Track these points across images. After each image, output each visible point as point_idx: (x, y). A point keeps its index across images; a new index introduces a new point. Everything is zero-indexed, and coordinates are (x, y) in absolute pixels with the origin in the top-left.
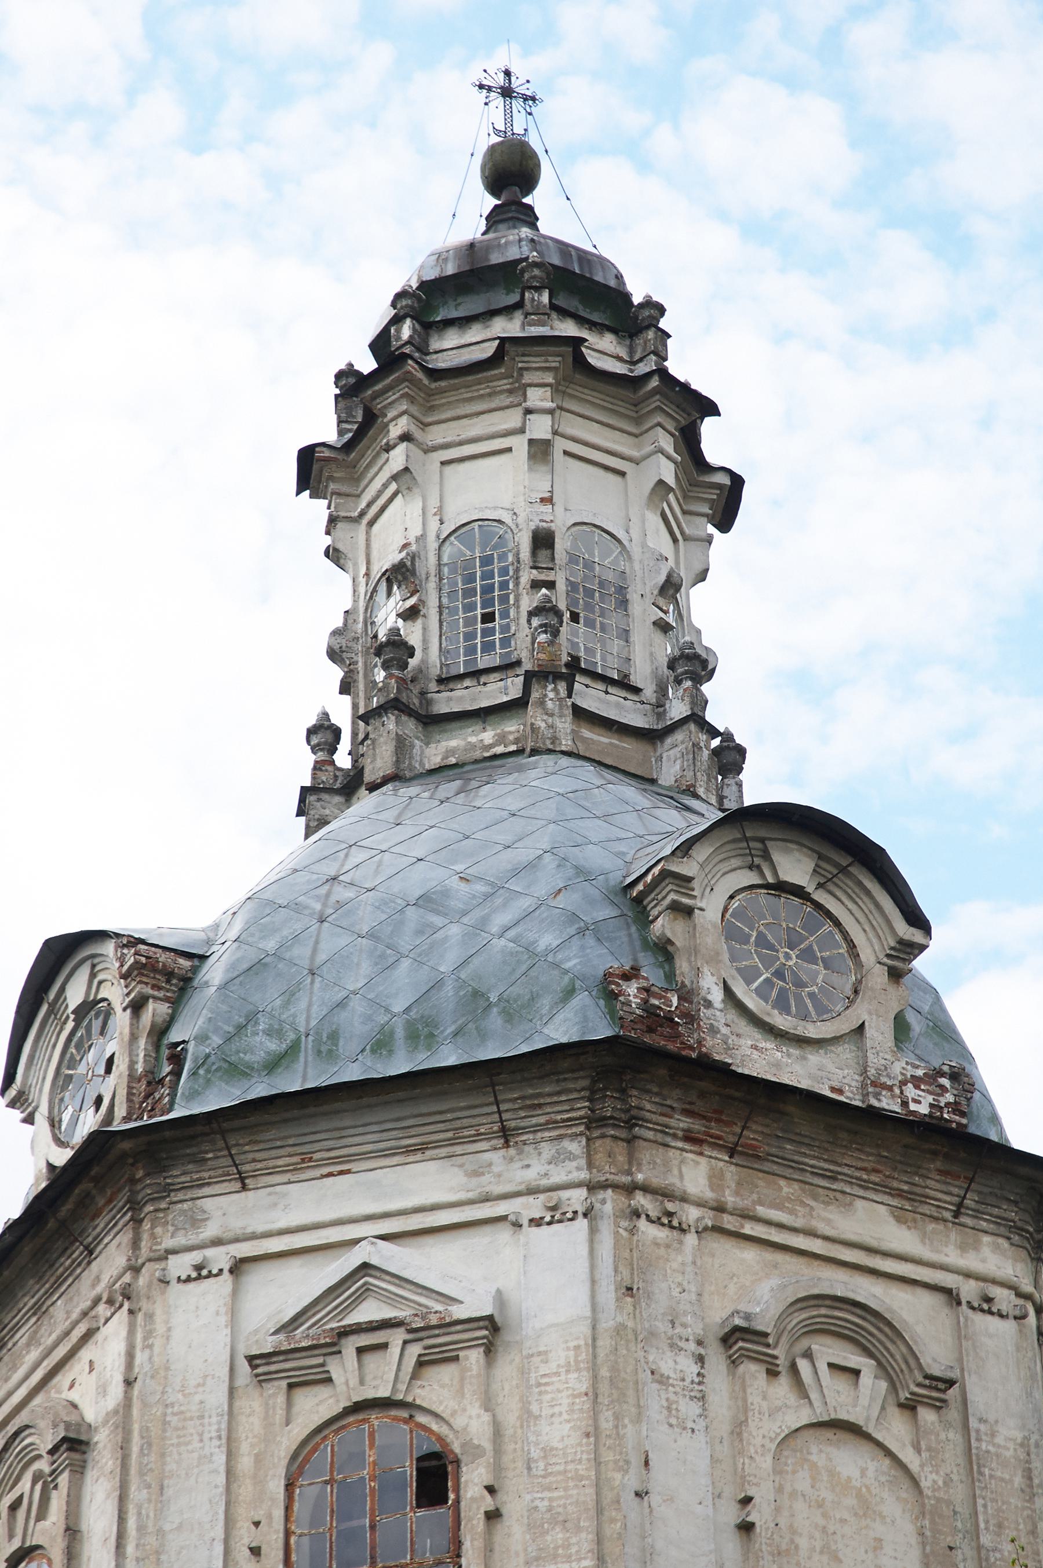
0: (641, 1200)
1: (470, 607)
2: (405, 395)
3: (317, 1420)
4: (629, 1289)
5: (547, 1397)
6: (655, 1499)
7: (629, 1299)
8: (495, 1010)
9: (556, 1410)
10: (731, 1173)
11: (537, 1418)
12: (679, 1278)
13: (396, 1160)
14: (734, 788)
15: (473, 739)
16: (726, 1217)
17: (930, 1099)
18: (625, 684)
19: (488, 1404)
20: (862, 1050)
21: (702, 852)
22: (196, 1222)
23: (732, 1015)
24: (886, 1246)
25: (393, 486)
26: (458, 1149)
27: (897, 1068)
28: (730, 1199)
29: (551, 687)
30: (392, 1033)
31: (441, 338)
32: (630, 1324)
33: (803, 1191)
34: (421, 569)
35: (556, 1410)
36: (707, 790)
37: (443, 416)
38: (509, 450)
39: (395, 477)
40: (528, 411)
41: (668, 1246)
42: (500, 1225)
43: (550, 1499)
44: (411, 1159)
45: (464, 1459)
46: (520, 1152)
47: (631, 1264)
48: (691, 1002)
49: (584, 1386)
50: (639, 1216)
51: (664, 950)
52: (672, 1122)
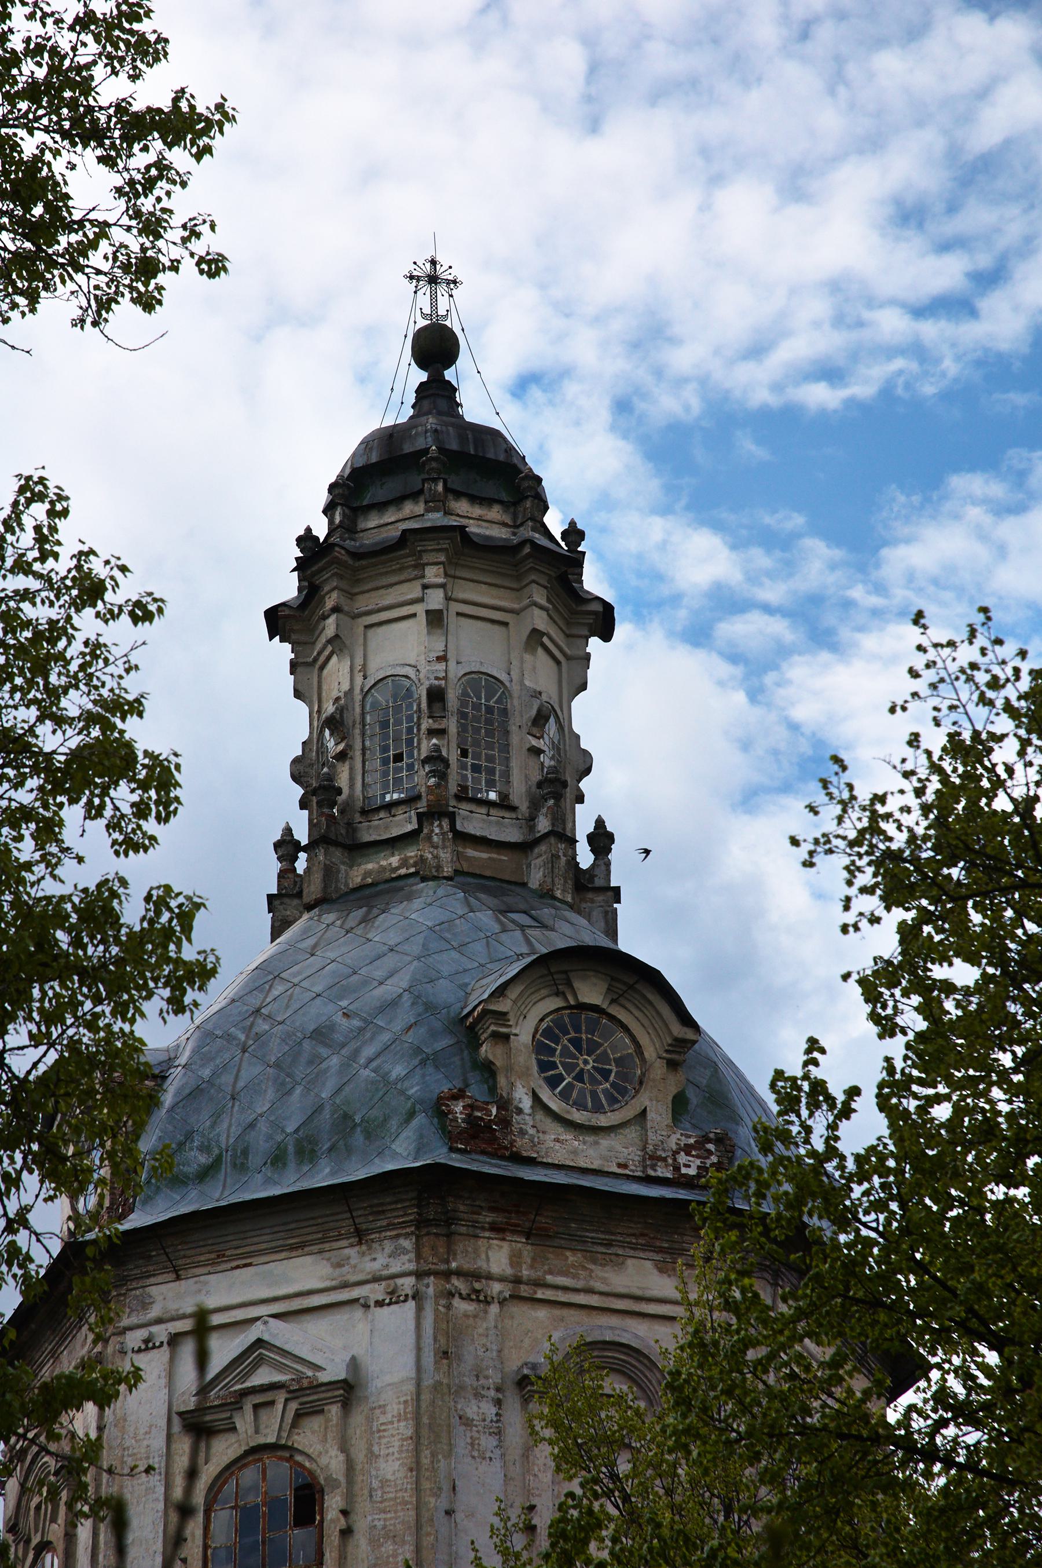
0: (457, 1283)
1: (385, 749)
2: (335, 574)
3: (226, 1460)
4: (446, 1353)
5: (384, 1441)
6: (459, 1516)
7: (445, 1361)
8: (359, 1129)
9: (391, 1450)
10: (527, 1251)
11: (378, 1457)
12: (484, 1340)
13: (283, 1255)
14: (603, 868)
15: (384, 863)
16: (523, 1287)
17: (698, 1162)
18: (504, 804)
19: (344, 1448)
20: (644, 1129)
21: (513, 993)
22: (145, 1305)
23: (540, 1116)
24: (649, 1293)
25: (330, 648)
26: (327, 1246)
27: (672, 1143)
28: (525, 1273)
29: (436, 823)
30: (286, 1149)
31: (366, 519)
32: (445, 1381)
33: (585, 1257)
34: (348, 719)
35: (391, 1450)
36: (564, 891)
37: (366, 588)
38: (414, 615)
39: (329, 641)
40: (425, 587)
41: (475, 1317)
42: (356, 1306)
43: (385, 1520)
44: (294, 1254)
45: (326, 1489)
46: (370, 1248)
47: (447, 1333)
48: (507, 1110)
49: (409, 1432)
50: (453, 1296)
51: (488, 1070)
52: (481, 1218)
